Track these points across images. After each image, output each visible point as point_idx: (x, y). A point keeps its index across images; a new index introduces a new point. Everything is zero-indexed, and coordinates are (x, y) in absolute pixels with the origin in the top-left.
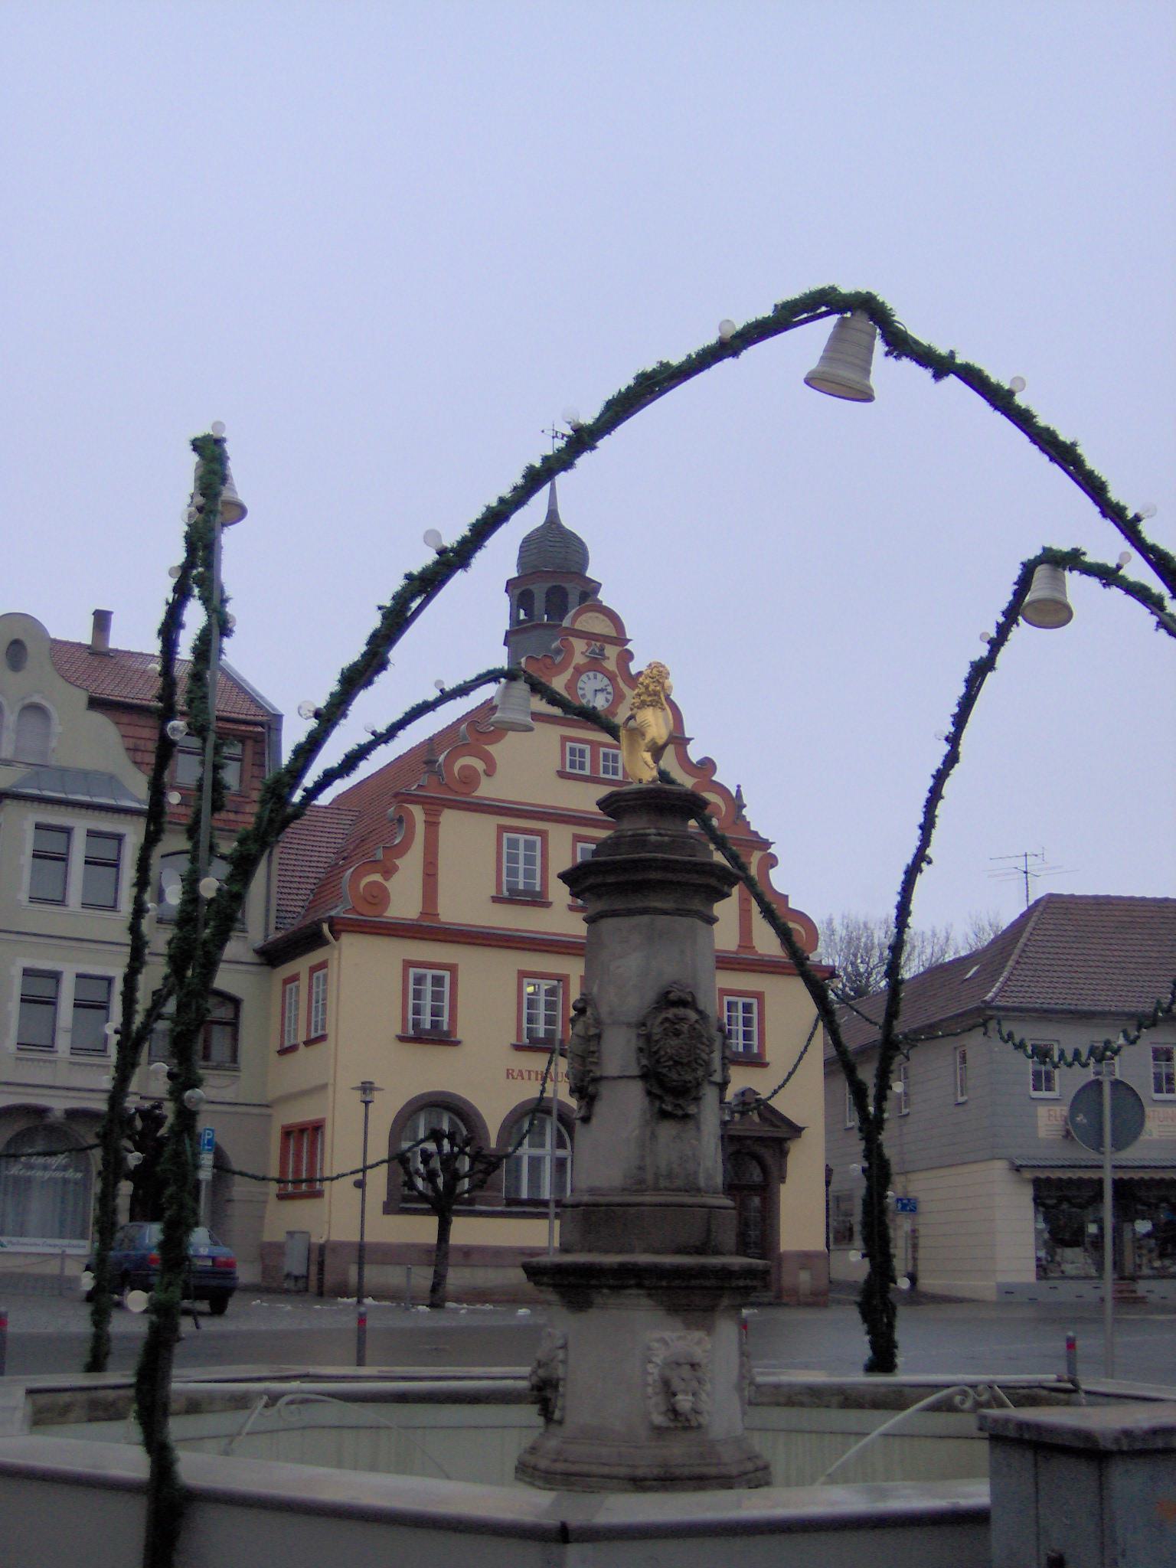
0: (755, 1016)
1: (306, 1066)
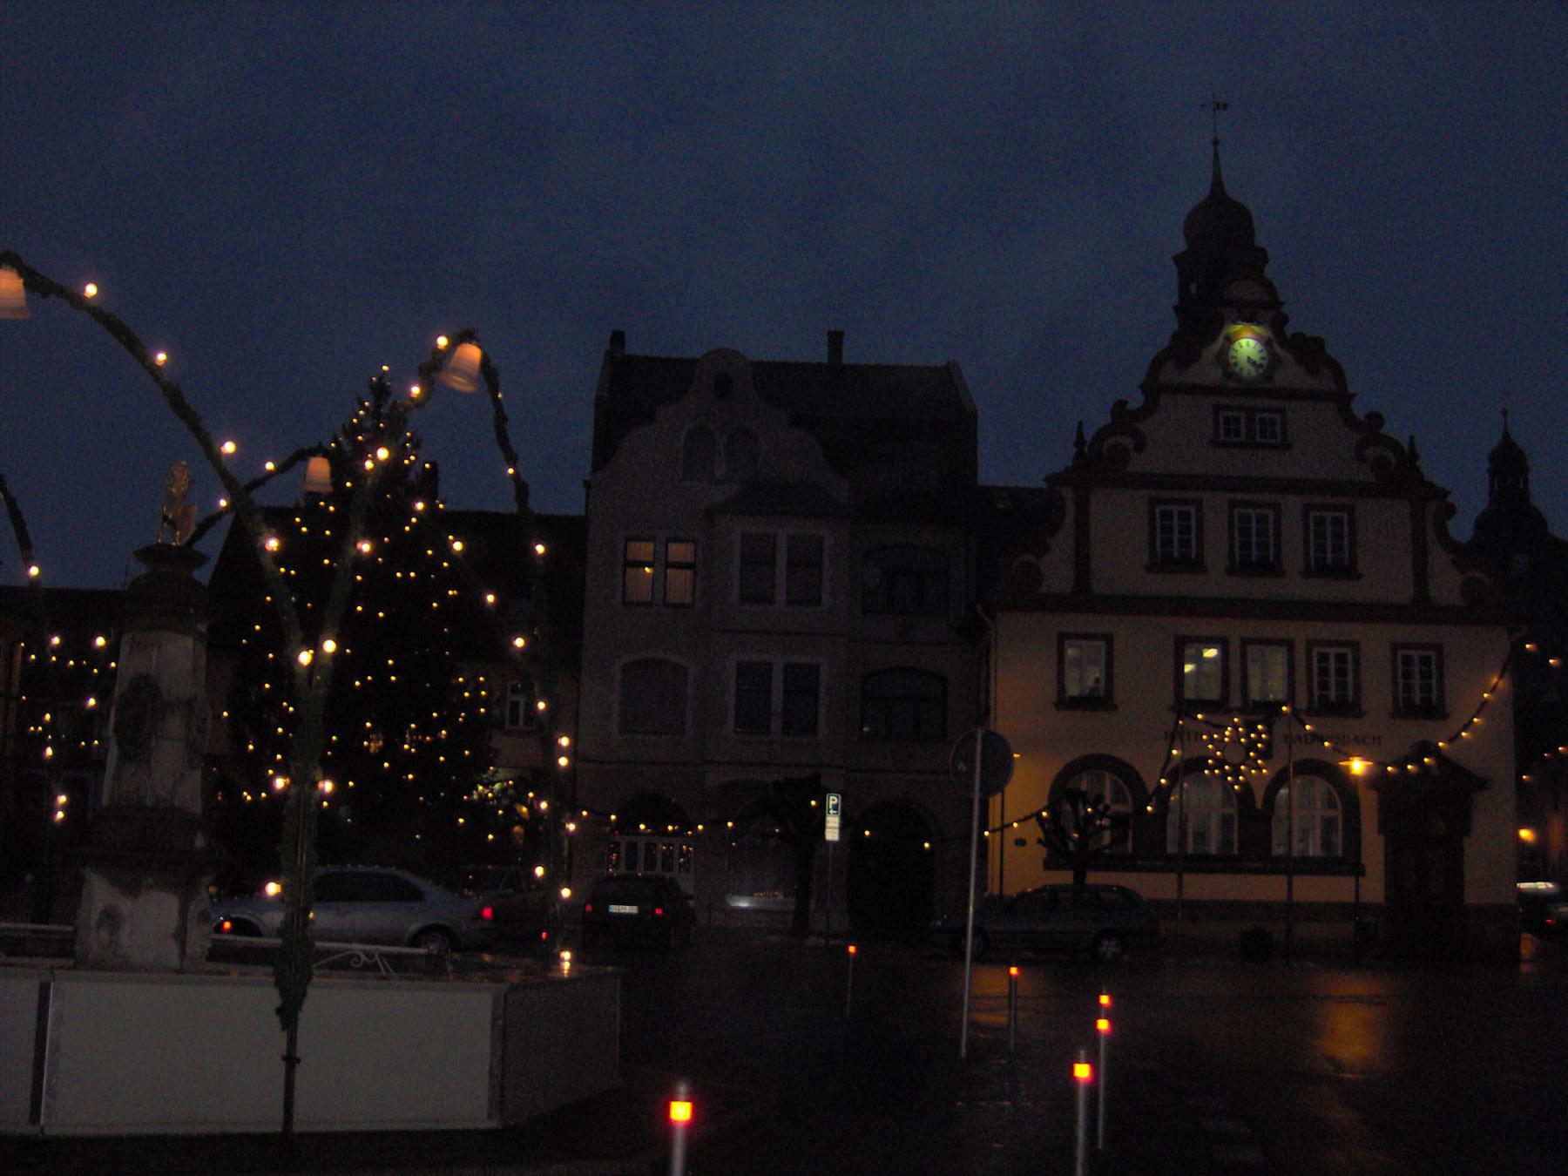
0: (1350, 666)
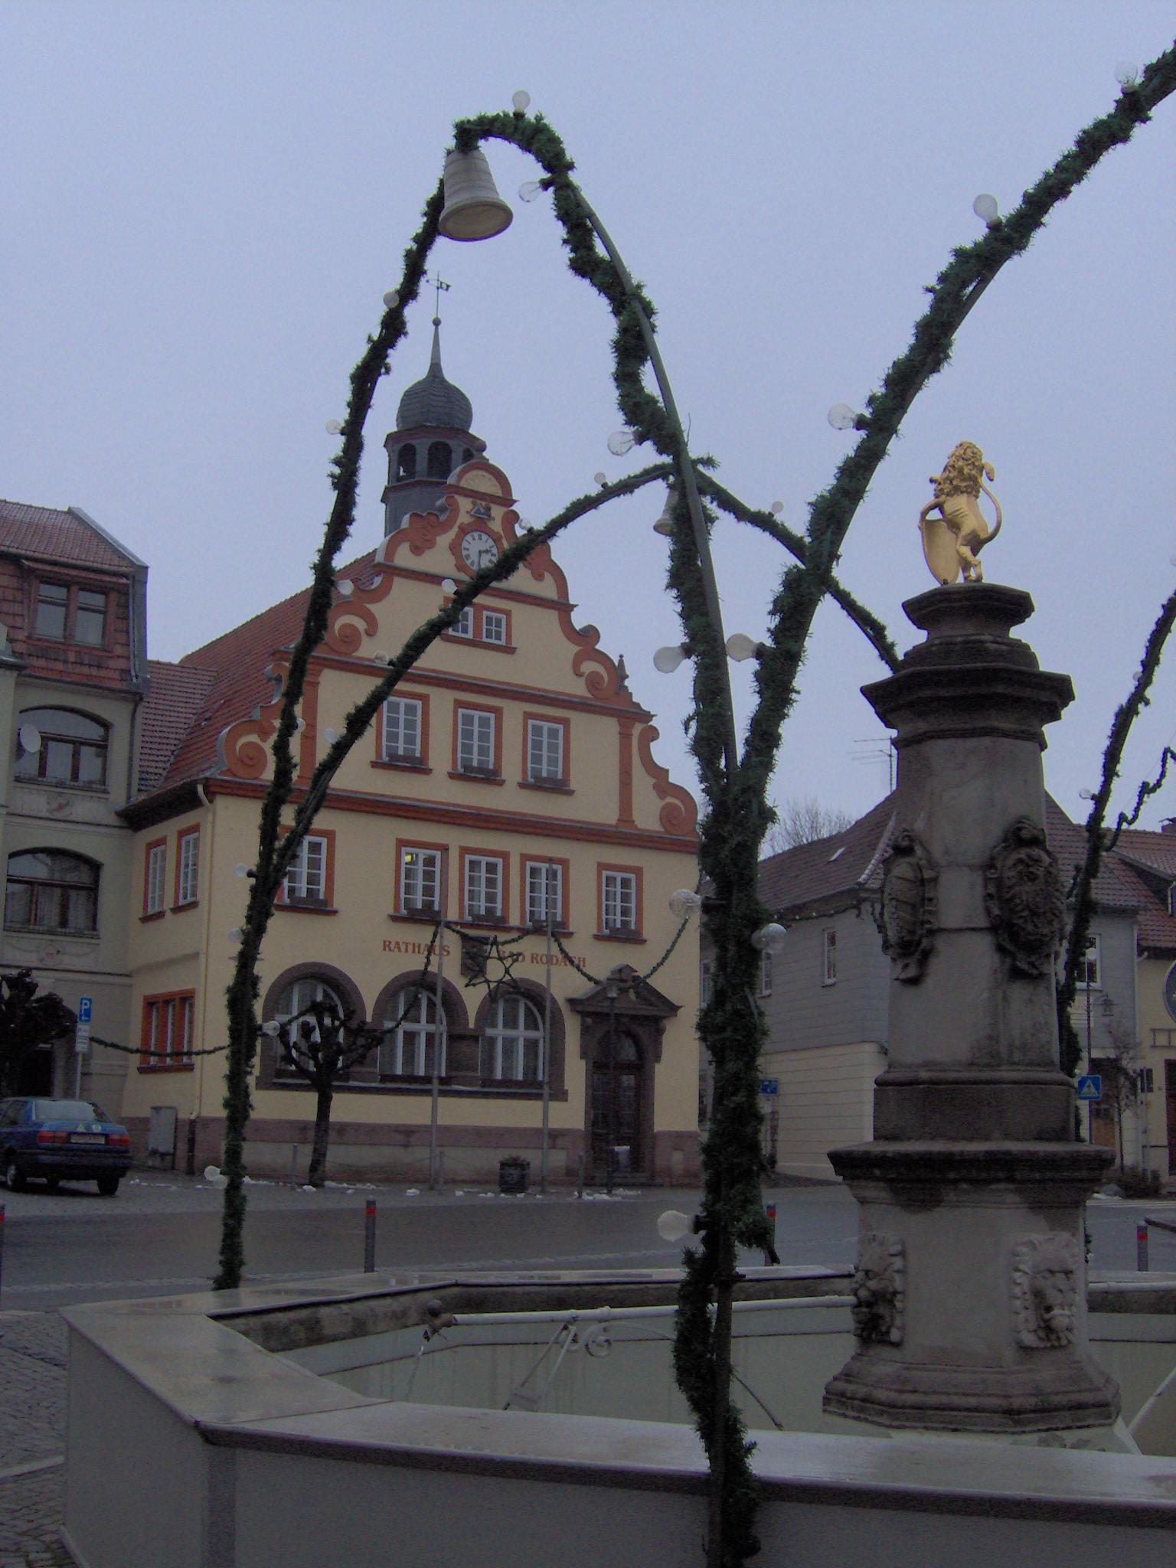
1: (174, 935)
